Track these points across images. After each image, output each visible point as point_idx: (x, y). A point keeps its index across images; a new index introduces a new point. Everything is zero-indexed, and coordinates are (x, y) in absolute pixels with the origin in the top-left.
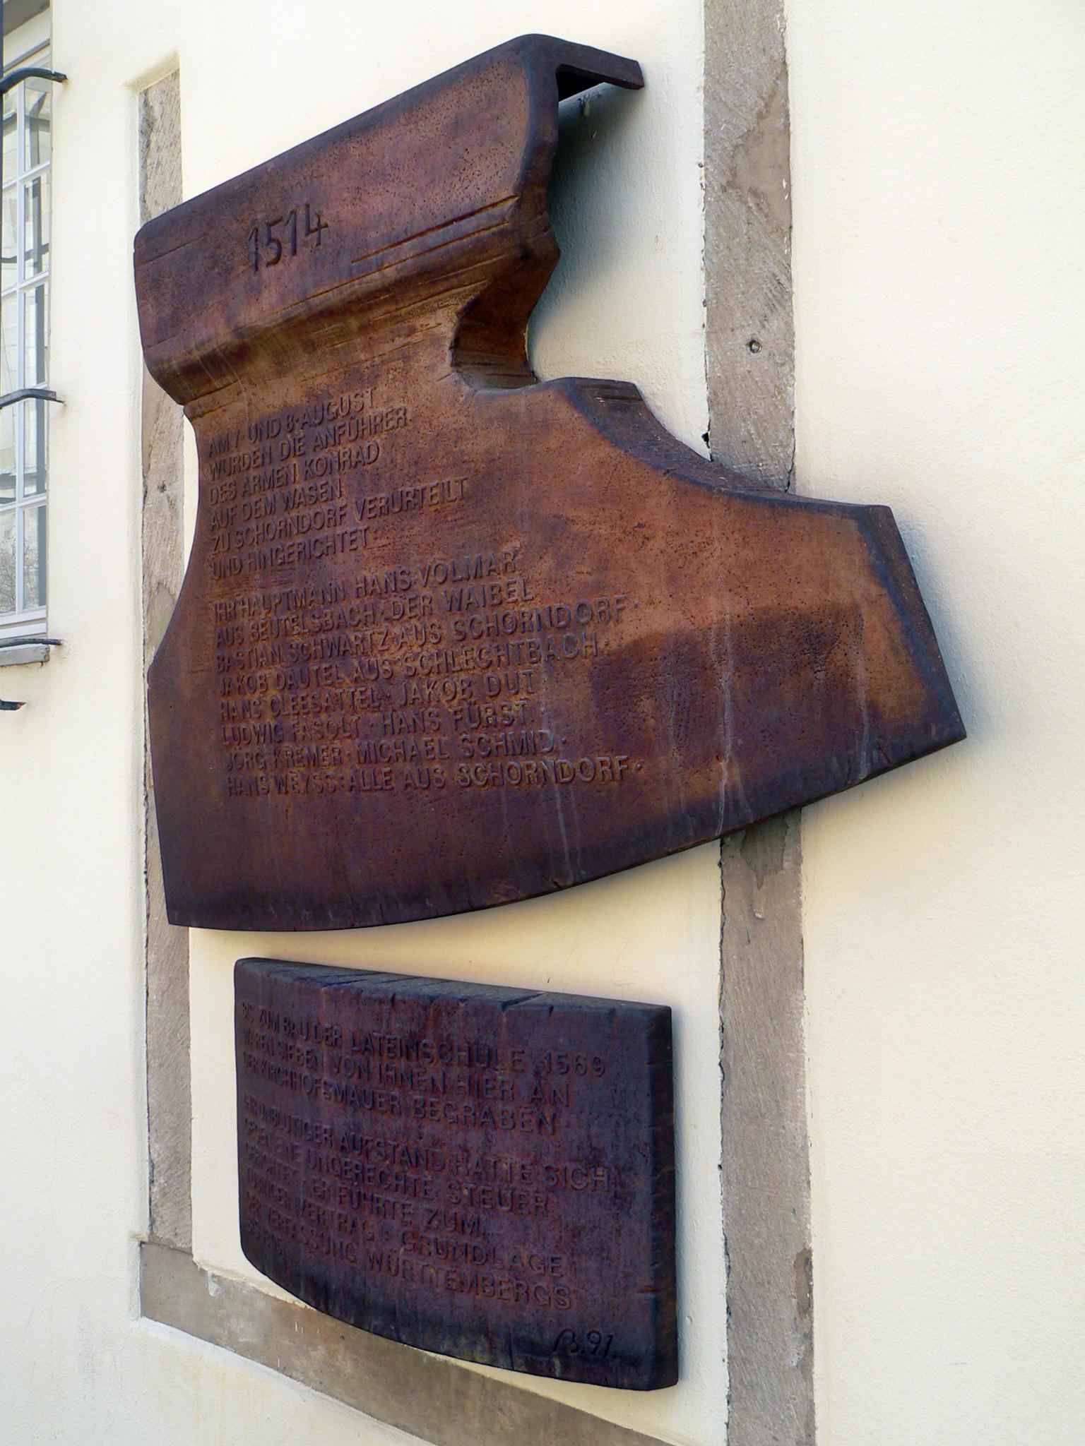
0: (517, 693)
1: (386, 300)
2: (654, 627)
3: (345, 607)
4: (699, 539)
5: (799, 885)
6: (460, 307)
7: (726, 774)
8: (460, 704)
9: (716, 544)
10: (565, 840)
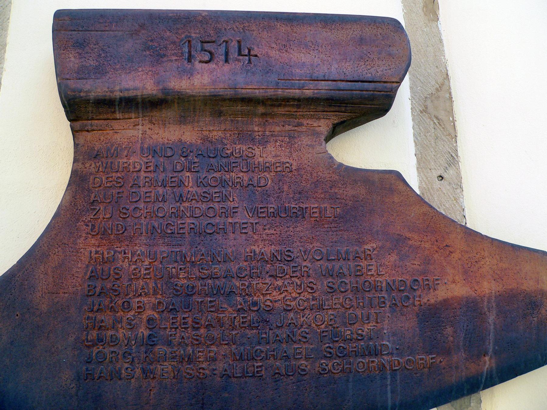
0: (369, 323)
1: (293, 105)
2: (456, 294)
3: (234, 267)
4: (478, 256)
6: (336, 122)
7: (488, 363)
8: (326, 327)
9: (487, 259)
10: (389, 400)
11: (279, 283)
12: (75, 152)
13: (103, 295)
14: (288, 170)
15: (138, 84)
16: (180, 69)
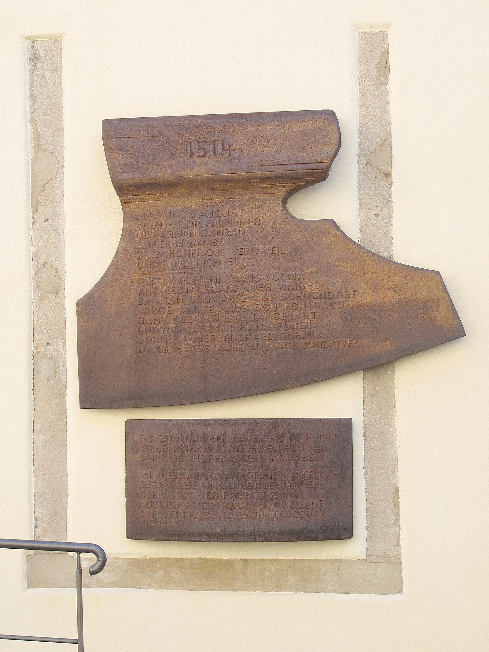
5: (394, 379)
11: (252, 294)
12: (124, 216)
13: (147, 304)
14: (257, 223)
15: (160, 174)
16: (186, 163)
